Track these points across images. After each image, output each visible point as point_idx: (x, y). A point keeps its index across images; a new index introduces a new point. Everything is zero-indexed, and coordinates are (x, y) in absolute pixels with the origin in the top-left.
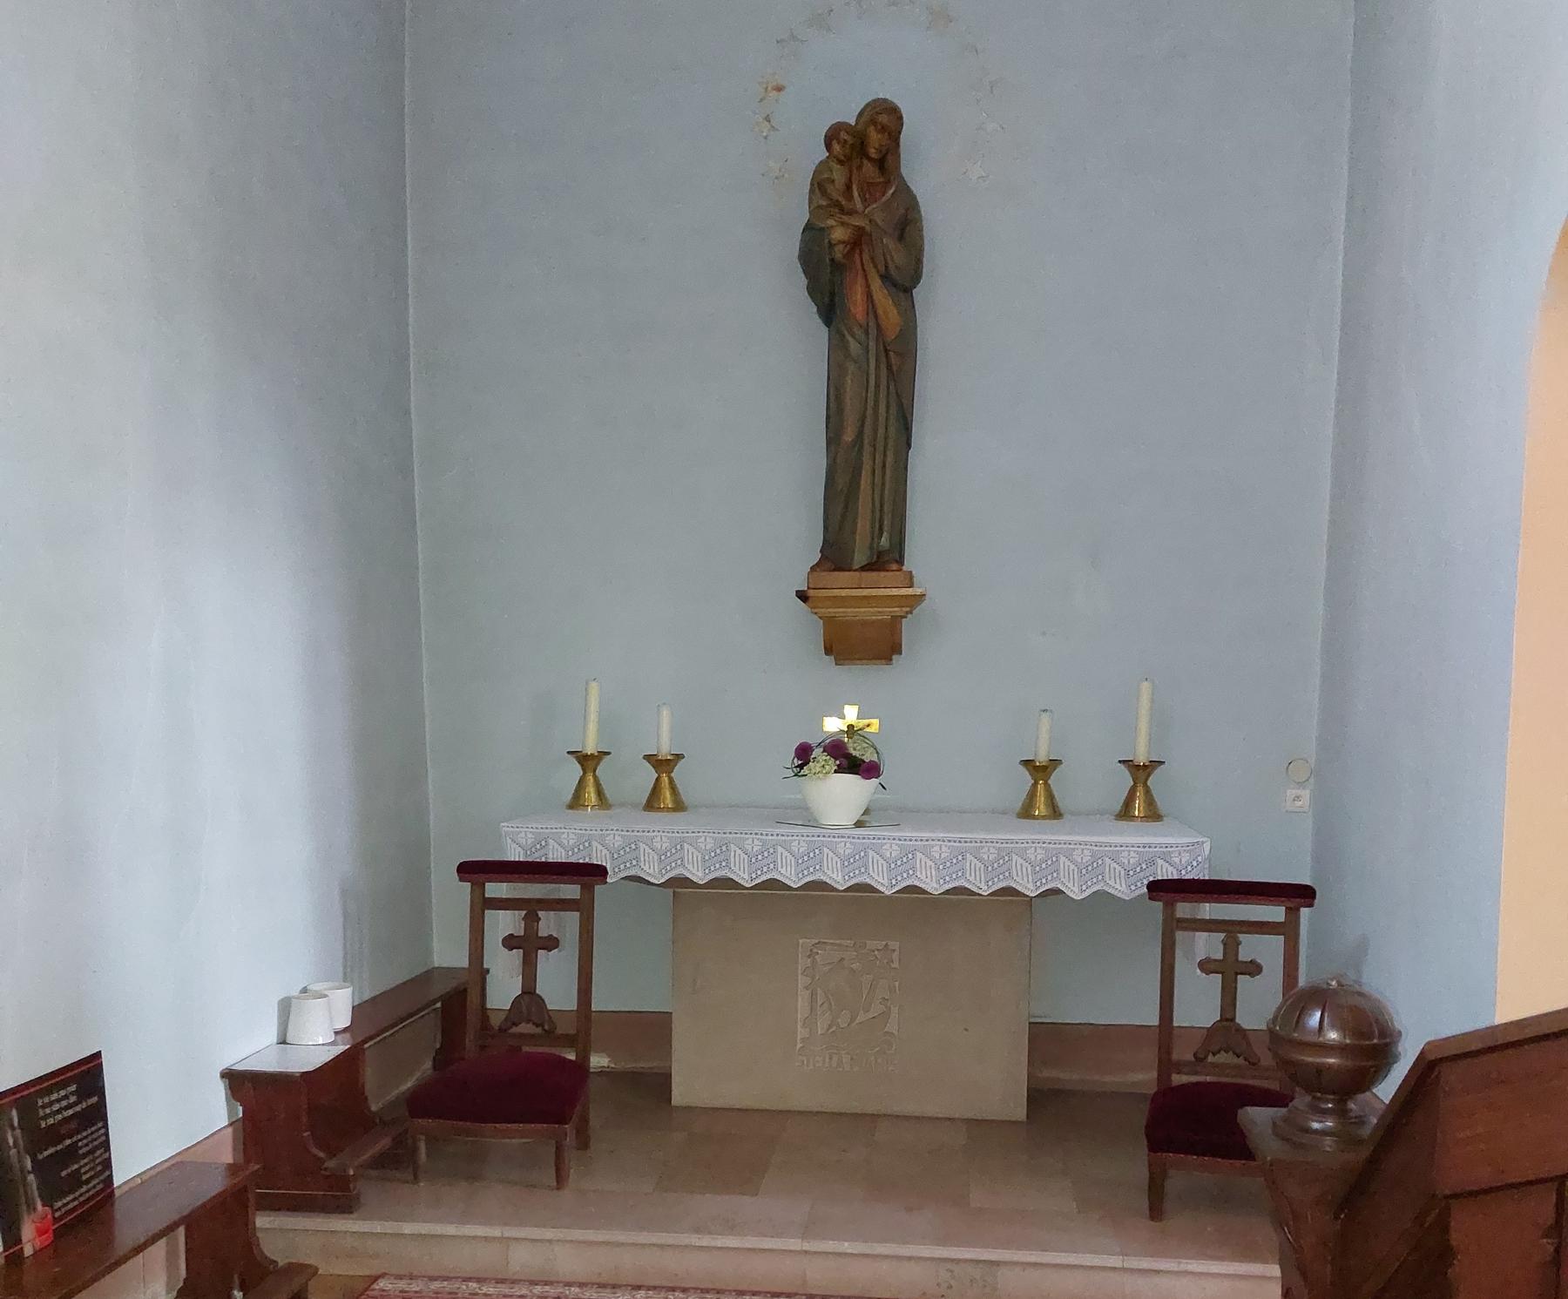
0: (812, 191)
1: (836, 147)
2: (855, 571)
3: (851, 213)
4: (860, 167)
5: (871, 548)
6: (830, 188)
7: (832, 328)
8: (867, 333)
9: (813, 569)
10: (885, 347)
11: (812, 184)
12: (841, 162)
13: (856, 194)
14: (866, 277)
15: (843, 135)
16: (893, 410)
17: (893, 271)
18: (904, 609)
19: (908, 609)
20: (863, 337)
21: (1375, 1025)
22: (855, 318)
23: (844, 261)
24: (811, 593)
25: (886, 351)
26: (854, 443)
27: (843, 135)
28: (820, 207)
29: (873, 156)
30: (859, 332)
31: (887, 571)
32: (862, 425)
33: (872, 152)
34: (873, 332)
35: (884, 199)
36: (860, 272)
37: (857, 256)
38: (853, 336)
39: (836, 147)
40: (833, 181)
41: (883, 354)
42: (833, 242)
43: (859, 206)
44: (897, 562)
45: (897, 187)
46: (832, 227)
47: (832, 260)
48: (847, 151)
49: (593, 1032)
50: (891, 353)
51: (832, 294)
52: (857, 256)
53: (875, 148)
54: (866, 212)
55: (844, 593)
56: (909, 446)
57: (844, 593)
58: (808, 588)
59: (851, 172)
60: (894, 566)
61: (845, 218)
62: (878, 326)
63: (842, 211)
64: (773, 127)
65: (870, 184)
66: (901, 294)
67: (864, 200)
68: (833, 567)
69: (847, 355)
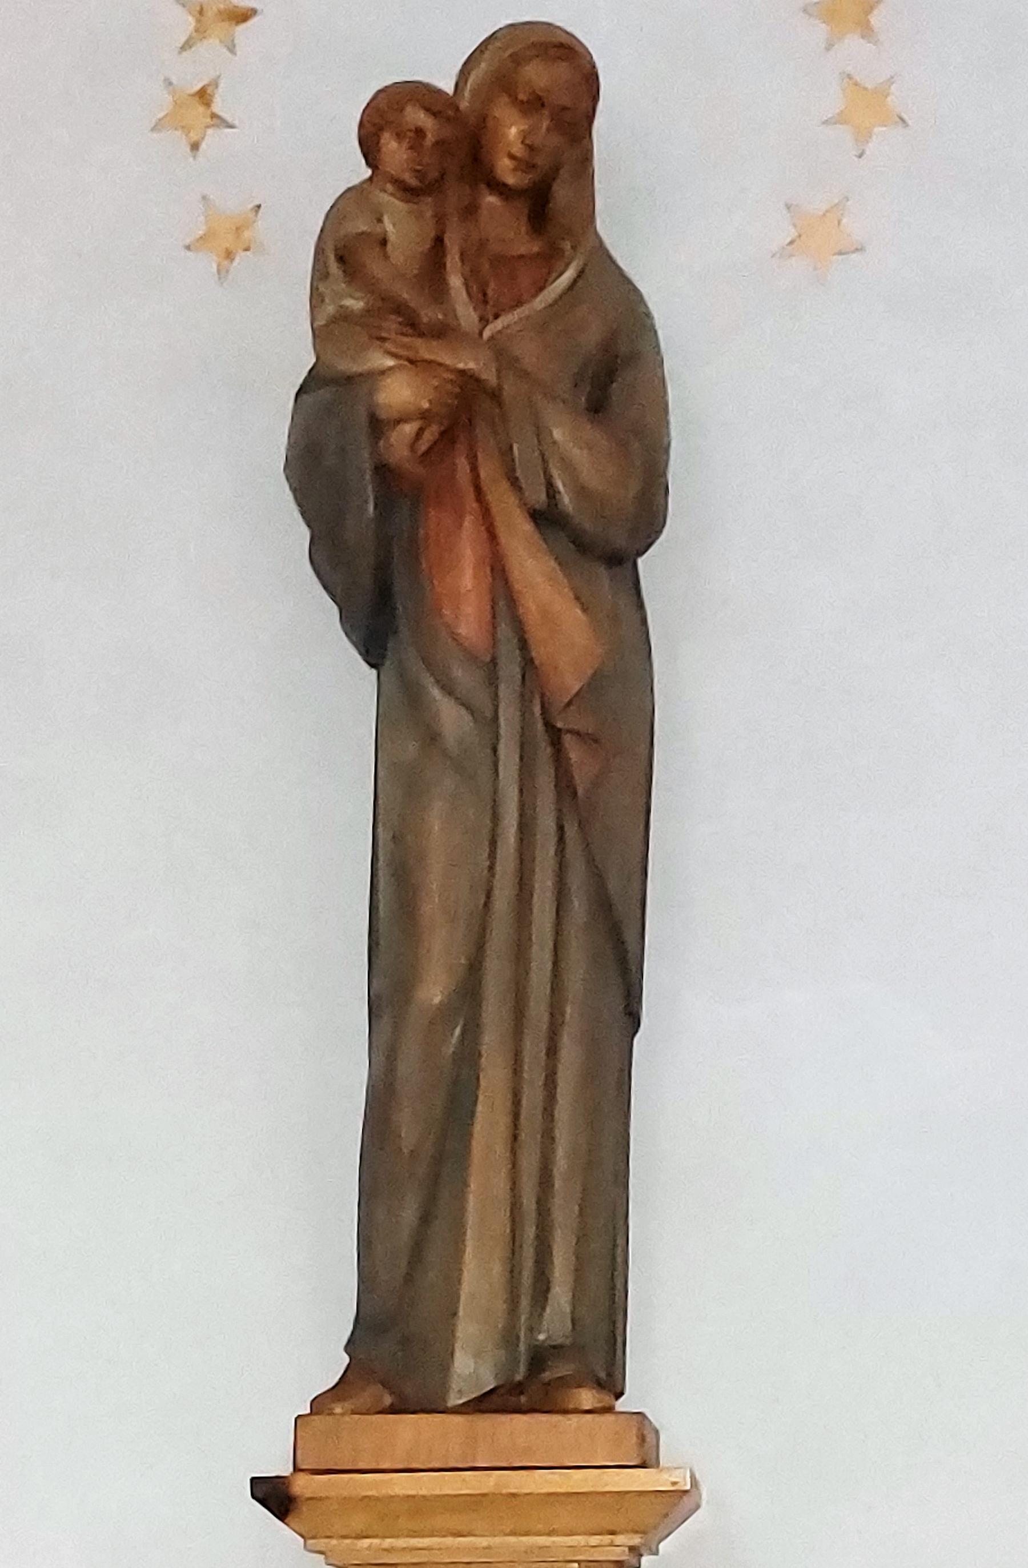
0: (320, 273)
1: (391, 147)
2: (457, 1410)
3: (441, 332)
4: (470, 211)
5: (509, 1338)
6: (376, 268)
7: (384, 669)
8: (492, 680)
9: (319, 1405)
10: (549, 725)
11: (319, 251)
12: (408, 192)
13: (455, 281)
14: (486, 513)
15: (417, 116)
16: (578, 906)
17: (566, 500)
18: (619, 1539)
19: (636, 1540)
20: (481, 698)
21: (655, 506)
22: (455, 637)
23: (420, 470)
24: (303, 1486)
25: (555, 735)
26: (445, 1014)
27: (417, 116)
28: (343, 317)
29: (511, 180)
30: (461, 674)
31: (566, 1412)
32: (480, 947)
33: (506, 170)
34: (510, 669)
35: (540, 302)
36: (471, 503)
37: (462, 464)
38: (448, 690)
39: (391, 147)
40: (384, 242)
41: (544, 751)
42: (383, 415)
43: (466, 314)
44: (600, 1385)
45: (580, 274)
46: (383, 372)
47: (383, 471)
48: (426, 160)
49: (548, 991)
50: (568, 740)
51: (382, 572)
52: (462, 464)
53: (512, 157)
54: (487, 334)
55: (402, 1485)
56: (633, 1020)
57: (402, 1485)
58: (296, 1469)
59: (440, 220)
60: (587, 1398)
61: (426, 350)
62: (528, 664)
63: (412, 325)
64: (214, 116)
65: (499, 261)
66: (602, 571)
67: (481, 298)
68: (388, 1400)
69: (432, 738)
